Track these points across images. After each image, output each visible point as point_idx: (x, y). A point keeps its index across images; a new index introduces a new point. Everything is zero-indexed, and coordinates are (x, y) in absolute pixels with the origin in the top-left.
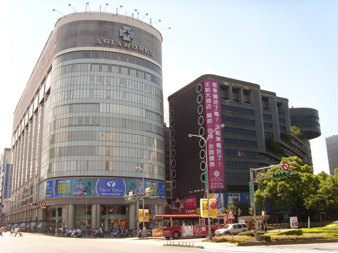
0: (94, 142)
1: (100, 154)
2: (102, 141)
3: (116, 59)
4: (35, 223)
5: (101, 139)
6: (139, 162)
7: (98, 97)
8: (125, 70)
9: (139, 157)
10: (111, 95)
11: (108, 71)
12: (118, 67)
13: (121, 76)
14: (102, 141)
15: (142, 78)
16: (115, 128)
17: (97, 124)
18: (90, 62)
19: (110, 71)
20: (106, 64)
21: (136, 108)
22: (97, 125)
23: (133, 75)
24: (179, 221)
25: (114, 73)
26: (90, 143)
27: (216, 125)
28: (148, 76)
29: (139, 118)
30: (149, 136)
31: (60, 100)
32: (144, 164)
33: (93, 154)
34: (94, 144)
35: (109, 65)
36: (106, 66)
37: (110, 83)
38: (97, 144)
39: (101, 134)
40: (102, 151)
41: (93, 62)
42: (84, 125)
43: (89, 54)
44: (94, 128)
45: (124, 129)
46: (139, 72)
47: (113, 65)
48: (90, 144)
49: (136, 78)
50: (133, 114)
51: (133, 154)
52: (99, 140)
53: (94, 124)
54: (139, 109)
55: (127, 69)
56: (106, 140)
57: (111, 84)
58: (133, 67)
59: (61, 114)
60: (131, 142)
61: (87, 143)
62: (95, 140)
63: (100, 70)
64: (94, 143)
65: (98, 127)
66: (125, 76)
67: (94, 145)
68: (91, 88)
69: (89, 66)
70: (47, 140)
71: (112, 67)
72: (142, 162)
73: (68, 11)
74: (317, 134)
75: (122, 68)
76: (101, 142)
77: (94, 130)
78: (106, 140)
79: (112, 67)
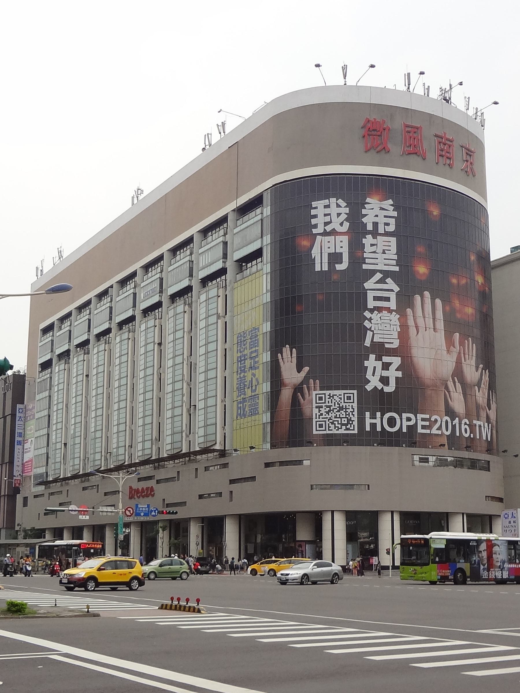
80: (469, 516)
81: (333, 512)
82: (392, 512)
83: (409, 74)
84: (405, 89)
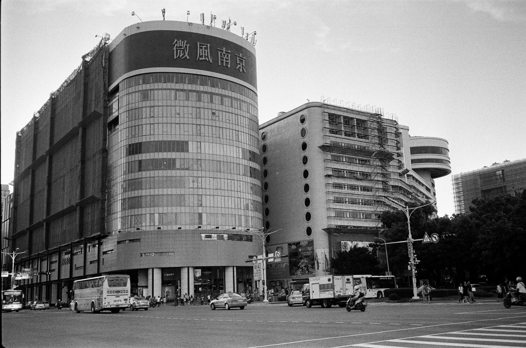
0: (183, 190)
3: (183, 82)
4: (300, 300)
5: (191, 186)
7: (186, 133)
8: (217, 99)
10: (202, 131)
14: (193, 188)
16: (207, 173)
18: (174, 88)
19: (199, 100)
20: (194, 91)
22: (187, 169)
26: (178, 191)
29: (195, 155)
34: (183, 193)
35: (198, 92)
37: (154, 114)
40: (192, 200)
41: (178, 88)
42: (178, 169)
43: (173, 77)
45: (219, 174)
46: (234, 100)
47: (202, 92)
49: (231, 108)
51: (230, 204)
54: (235, 148)
55: (209, 96)
56: (231, 190)
57: (202, 117)
58: (217, 92)
61: (174, 191)
62: (184, 187)
63: (187, 99)
65: (187, 171)
66: (206, 104)
67: (183, 193)
68: (151, 122)
69: (173, 92)
70: (387, 209)
71: (202, 95)
72: (200, 212)
73: (134, 21)
74: (444, 172)
78: (197, 188)
79: (202, 95)
80: (238, 268)
81: (153, 269)
82: (188, 267)
83: (203, 14)
84: (201, 23)
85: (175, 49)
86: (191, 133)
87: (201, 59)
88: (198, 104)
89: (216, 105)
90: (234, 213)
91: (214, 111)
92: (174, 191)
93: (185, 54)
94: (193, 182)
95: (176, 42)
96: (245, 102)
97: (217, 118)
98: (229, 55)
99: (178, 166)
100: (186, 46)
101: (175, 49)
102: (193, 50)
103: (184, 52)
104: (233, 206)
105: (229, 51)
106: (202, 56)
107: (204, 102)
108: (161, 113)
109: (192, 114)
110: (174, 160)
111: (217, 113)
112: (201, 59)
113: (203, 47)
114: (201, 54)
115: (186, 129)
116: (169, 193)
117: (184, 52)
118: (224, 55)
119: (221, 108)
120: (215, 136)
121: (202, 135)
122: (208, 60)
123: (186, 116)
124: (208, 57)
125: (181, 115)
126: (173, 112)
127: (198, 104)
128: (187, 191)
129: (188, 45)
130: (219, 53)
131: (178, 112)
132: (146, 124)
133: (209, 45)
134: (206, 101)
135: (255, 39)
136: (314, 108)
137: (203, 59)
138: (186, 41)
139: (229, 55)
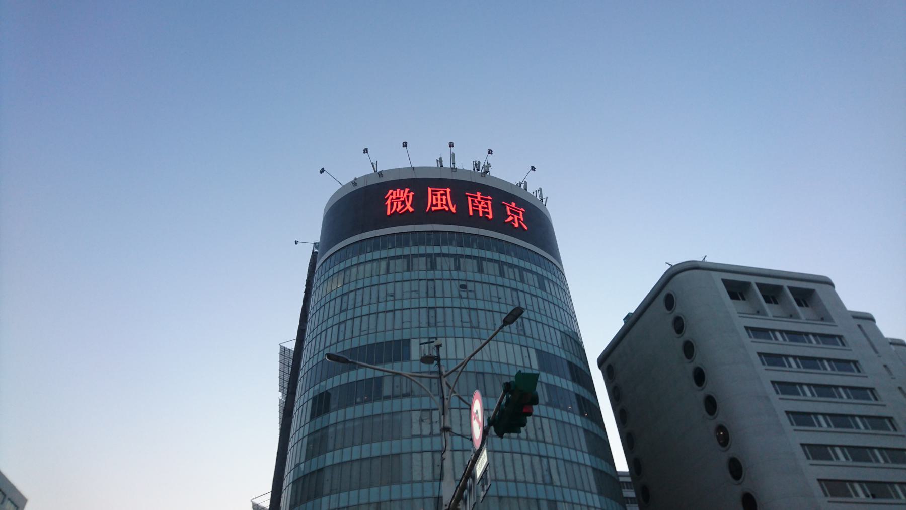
1: (416, 477)
2: (421, 436)
3: (407, 244)
5: (416, 431)
6: (542, 495)
7: (407, 325)
8: (471, 265)
9: (539, 479)
11: (429, 267)
12: (452, 259)
13: (462, 275)
14: (421, 436)
15: (515, 280)
17: (404, 392)
19: (433, 267)
21: (509, 346)
22: (407, 395)
23: (491, 272)
24: (629, 480)
25: (465, 271)
27: (471, 213)
28: (528, 276)
30: (567, 457)
31: (359, 319)
32: (558, 504)
33: (394, 479)
36: (399, 261)
38: (406, 449)
39: (416, 416)
42: (387, 398)
44: (396, 405)
47: (462, 256)
48: (386, 452)
50: (503, 360)
52: (413, 436)
53: (397, 391)
54: (517, 348)
59: (377, 332)
60: (503, 478)
61: (377, 449)
64: (395, 446)
65: (406, 401)
71: (438, 259)
72: (551, 497)
75: (484, 263)
76: (416, 441)
77: (396, 408)
79: (438, 259)
85: (389, 202)
86: (415, 324)
87: (434, 209)
88: (430, 275)
89: (469, 269)
90: (533, 495)
91: (463, 283)
92: (377, 449)
93: (406, 206)
94: (421, 421)
95: (392, 194)
96: (530, 271)
97: (471, 295)
98: (489, 203)
99: (386, 390)
100: (408, 197)
101: (389, 202)
102: (420, 200)
103: (403, 203)
104: (530, 478)
105: (489, 198)
106: (437, 205)
107: (442, 270)
108: (372, 326)
109: (418, 292)
110: (379, 381)
111: (470, 286)
112: (434, 209)
113: (439, 193)
114: (435, 203)
115: (406, 318)
116: (366, 454)
117: (403, 203)
118: (480, 203)
119: (478, 277)
120: (468, 325)
121: (439, 324)
122: (447, 209)
123: (407, 295)
124: (447, 205)
125: (398, 296)
126: (382, 295)
127: (430, 275)
128: (406, 445)
129: (411, 194)
130: (470, 199)
131: (390, 290)
132: (422, 452)
133: (448, 190)
134: (445, 267)
135: (544, 197)
136: (686, 273)
137: (440, 208)
138: (407, 190)
139: (489, 203)
